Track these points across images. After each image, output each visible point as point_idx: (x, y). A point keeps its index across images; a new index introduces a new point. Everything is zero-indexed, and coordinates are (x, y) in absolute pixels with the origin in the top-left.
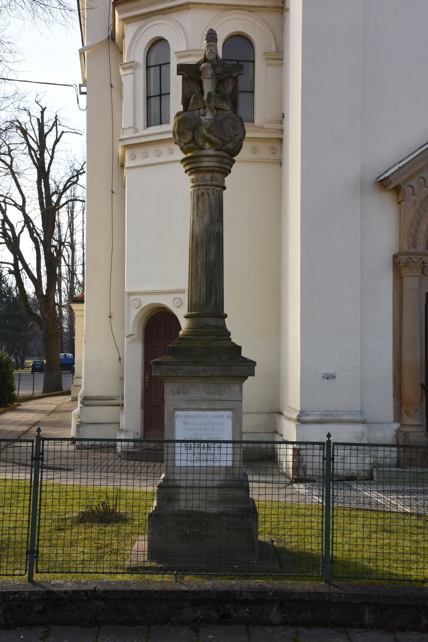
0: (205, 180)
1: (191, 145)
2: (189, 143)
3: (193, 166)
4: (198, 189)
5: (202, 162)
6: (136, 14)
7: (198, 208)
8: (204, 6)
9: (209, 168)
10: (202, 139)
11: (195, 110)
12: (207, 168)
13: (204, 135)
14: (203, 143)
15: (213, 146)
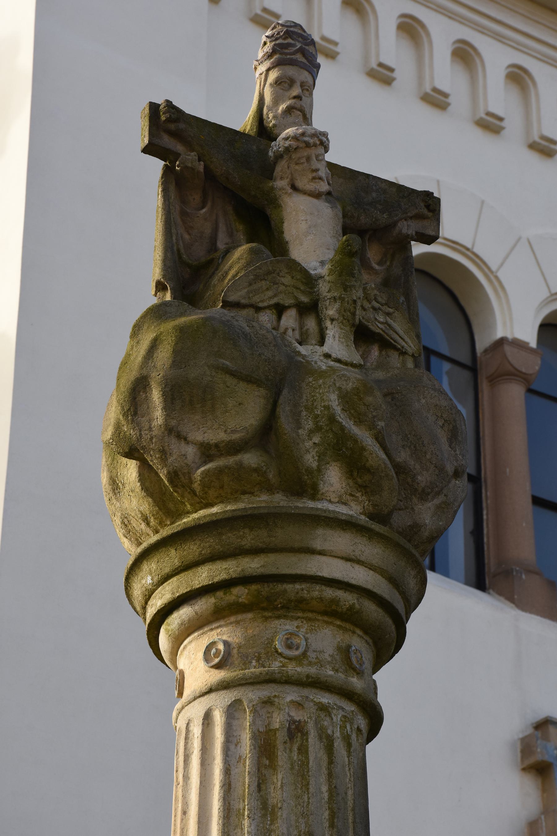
0: (312, 655)
1: (250, 459)
2: (234, 448)
3: (253, 565)
4: (268, 702)
5: (312, 552)
9: (340, 594)
11: (258, 309)
12: (329, 593)
13: (332, 419)
14: (321, 457)
15: (363, 488)
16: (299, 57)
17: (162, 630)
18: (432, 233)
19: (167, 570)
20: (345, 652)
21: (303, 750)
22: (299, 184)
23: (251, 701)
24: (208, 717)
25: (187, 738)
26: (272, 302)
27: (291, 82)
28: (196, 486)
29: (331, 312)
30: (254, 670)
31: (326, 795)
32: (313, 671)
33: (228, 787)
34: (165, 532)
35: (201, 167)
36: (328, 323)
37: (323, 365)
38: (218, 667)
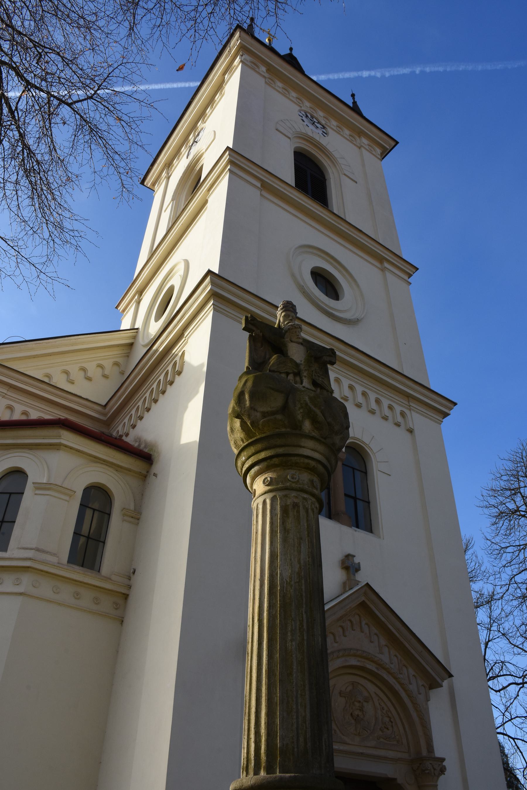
2: (273, 413)
3: (280, 451)
4: (286, 496)
5: (301, 447)
6: (160, 275)
7: (285, 530)
8: (74, 451)
9: (310, 461)
10: (301, 411)
11: (281, 373)
12: (306, 461)
13: (307, 404)
16: (291, 309)
17: (248, 476)
18: (334, 361)
19: (250, 454)
20: (312, 481)
21: (298, 512)
22: (293, 340)
23: (279, 496)
24: (264, 502)
25: (257, 509)
26: (285, 371)
27: (289, 316)
28: (260, 427)
29: (305, 374)
30: (280, 485)
31: (306, 527)
32: (301, 486)
33: (272, 523)
34: (250, 441)
35: (261, 334)
36: (304, 378)
37: (303, 389)
38: (268, 485)
